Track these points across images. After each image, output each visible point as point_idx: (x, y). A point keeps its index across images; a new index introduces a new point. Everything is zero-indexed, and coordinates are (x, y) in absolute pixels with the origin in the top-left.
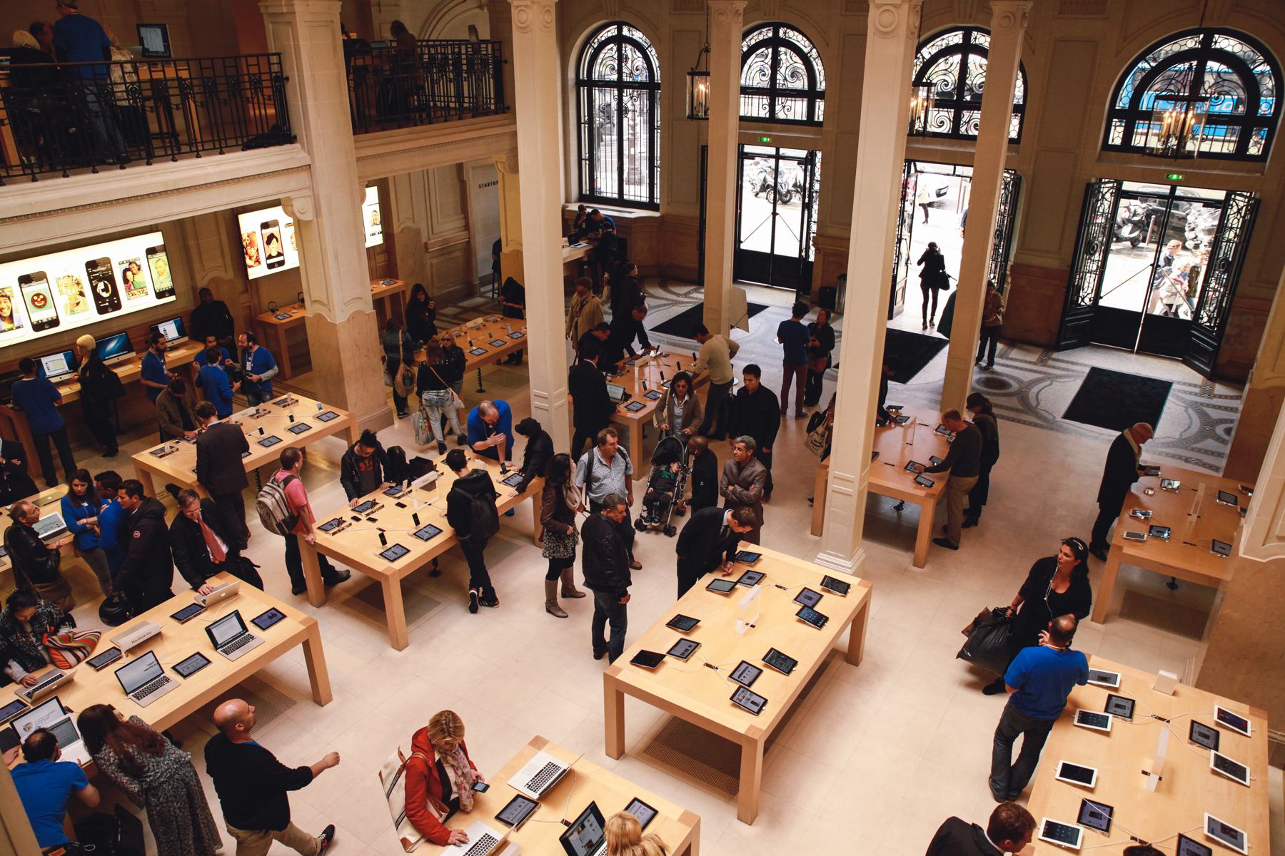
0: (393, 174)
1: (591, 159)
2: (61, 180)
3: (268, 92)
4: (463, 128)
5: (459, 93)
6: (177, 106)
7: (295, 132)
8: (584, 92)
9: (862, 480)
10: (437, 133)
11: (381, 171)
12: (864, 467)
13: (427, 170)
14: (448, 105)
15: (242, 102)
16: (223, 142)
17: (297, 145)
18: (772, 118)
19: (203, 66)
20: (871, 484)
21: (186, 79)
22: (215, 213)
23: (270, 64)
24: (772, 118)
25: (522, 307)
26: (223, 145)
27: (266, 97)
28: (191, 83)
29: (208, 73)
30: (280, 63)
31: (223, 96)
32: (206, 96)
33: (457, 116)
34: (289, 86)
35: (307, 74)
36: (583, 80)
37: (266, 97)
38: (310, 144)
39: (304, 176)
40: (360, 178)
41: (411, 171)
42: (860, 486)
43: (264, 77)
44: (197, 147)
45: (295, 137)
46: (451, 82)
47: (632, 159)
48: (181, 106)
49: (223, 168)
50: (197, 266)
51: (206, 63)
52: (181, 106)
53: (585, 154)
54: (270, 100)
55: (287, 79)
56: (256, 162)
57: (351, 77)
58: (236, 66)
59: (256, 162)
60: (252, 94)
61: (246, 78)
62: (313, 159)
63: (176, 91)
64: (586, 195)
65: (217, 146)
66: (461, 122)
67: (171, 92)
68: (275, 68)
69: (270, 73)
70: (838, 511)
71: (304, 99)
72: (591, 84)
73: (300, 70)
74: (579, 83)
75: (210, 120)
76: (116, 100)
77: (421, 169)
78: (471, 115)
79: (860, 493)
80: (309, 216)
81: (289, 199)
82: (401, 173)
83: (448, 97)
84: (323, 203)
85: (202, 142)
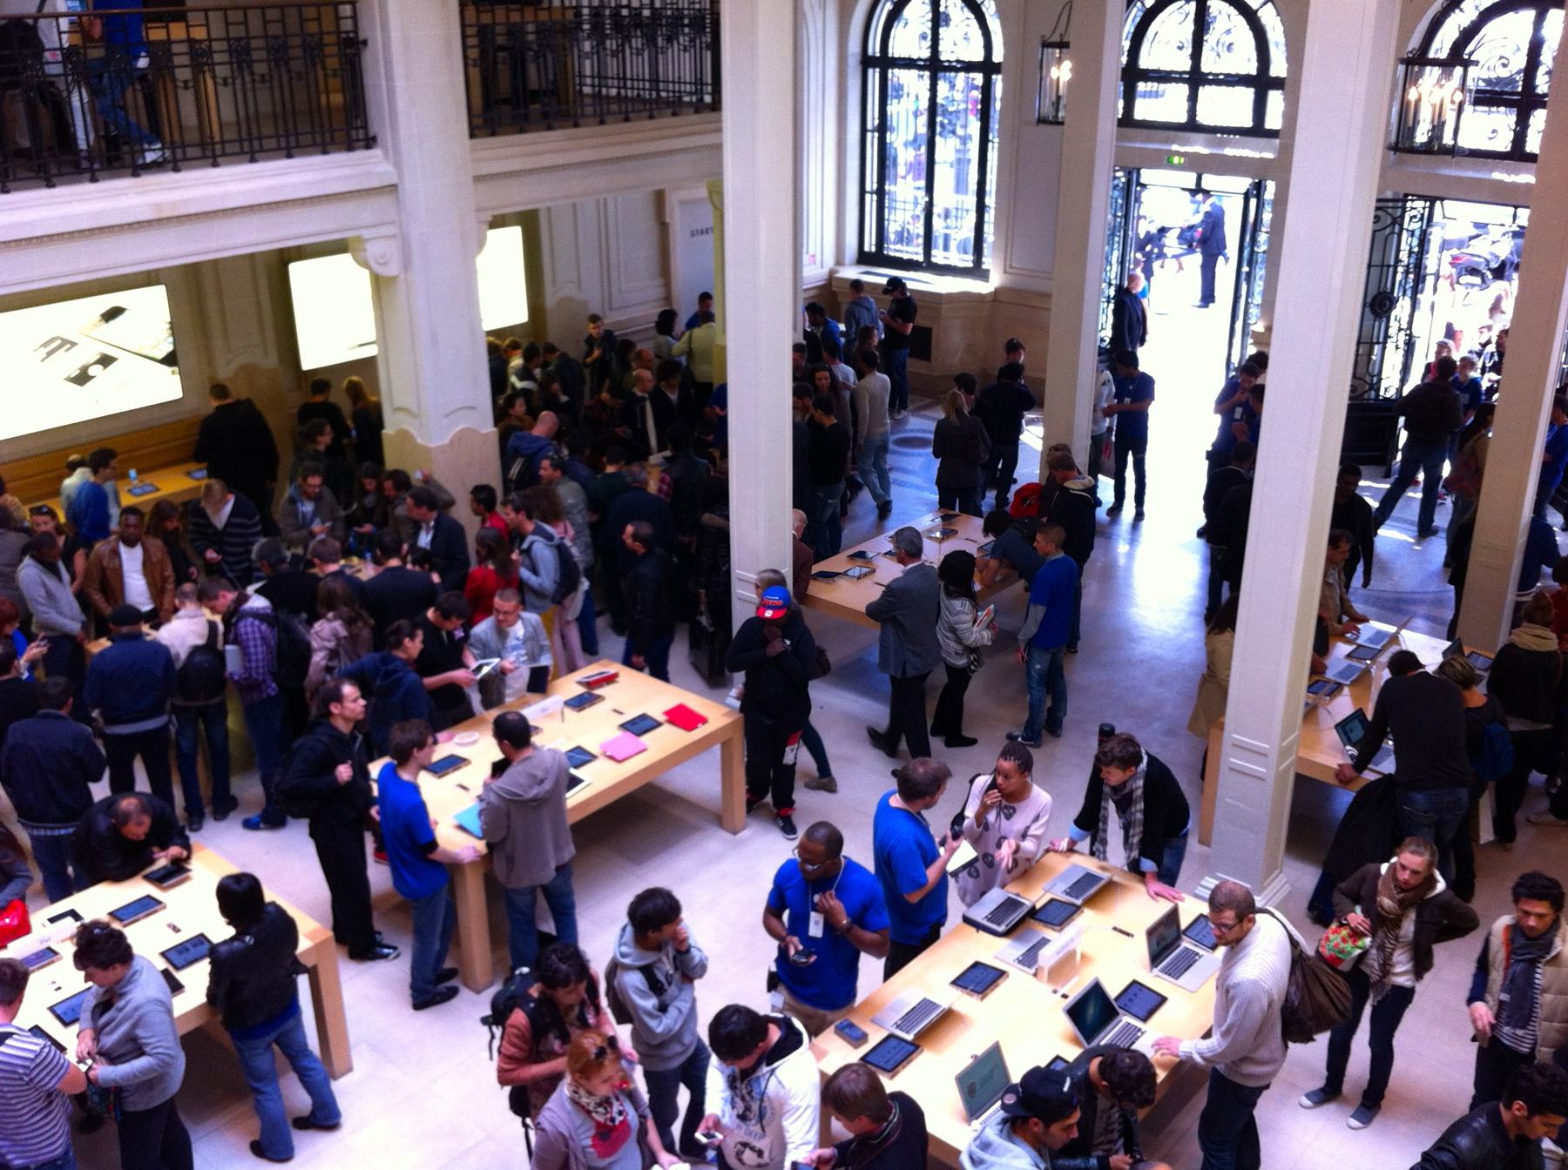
0: (548, 204)
1: (881, 193)
2: (43, 193)
3: (332, 63)
4: (656, 134)
5: (654, 77)
6: (186, 82)
7: (374, 129)
8: (874, 75)
9: (1284, 753)
10: (638, 136)
11: (520, 197)
12: (1285, 734)
13: (605, 200)
14: (600, 91)
15: (326, 76)
16: (292, 139)
17: (376, 152)
18: (1192, 126)
19: (230, 20)
20: (1300, 760)
21: (201, 41)
22: (252, 256)
23: (338, 18)
24: (1192, 126)
25: (117, 562)
26: (293, 144)
27: (294, 75)
28: (210, 47)
29: (275, 29)
30: (354, 17)
31: (260, 69)
32: (232, 70)
33: (647, 114)
34: (367, 56)
35: (395, 34)
36: (873, 58)
37: (294, 75)
38: (397, 153)
39: (386, 201)
40: (478, 210)
41: (577, 200)
42: (1280, 763)
43: (327, 39)
44: (213, 150)
45: (374, 139)
46: (685, 50)
47: (960, 187)
48: (191, 84)
49: (254, 184)
50: (218, 343)
51: (273, 14)
52: (191, 84)
53: (871, 183)
54: (335, 75)
55: (365, 43)
56: (309, 177)
57: (472, 41)
58: (227, 24)
59: (309, 177)
60: (68, 85)
61: (296, 41)
62: (401, 175)
63: (185, 60)
64: (870, 253)
65: (246, 149)
66: (652, 123)
67: (177, 60)
68: (347, 25)
69: (338, 32)
70: (1239, 804)
71: (390, 78)
72: (886, 62)
73: (385, 28)
74: (867, 62)
75: (237, 113)
76: (231, 63)
77: (570, 201)
78: (671, 111)
79: (1281, 776)
80: (391, 270)
81: (359, 239)
82: (560, 202)
83: (599, 77)
84: (416, 247)
85: (223, 142)
